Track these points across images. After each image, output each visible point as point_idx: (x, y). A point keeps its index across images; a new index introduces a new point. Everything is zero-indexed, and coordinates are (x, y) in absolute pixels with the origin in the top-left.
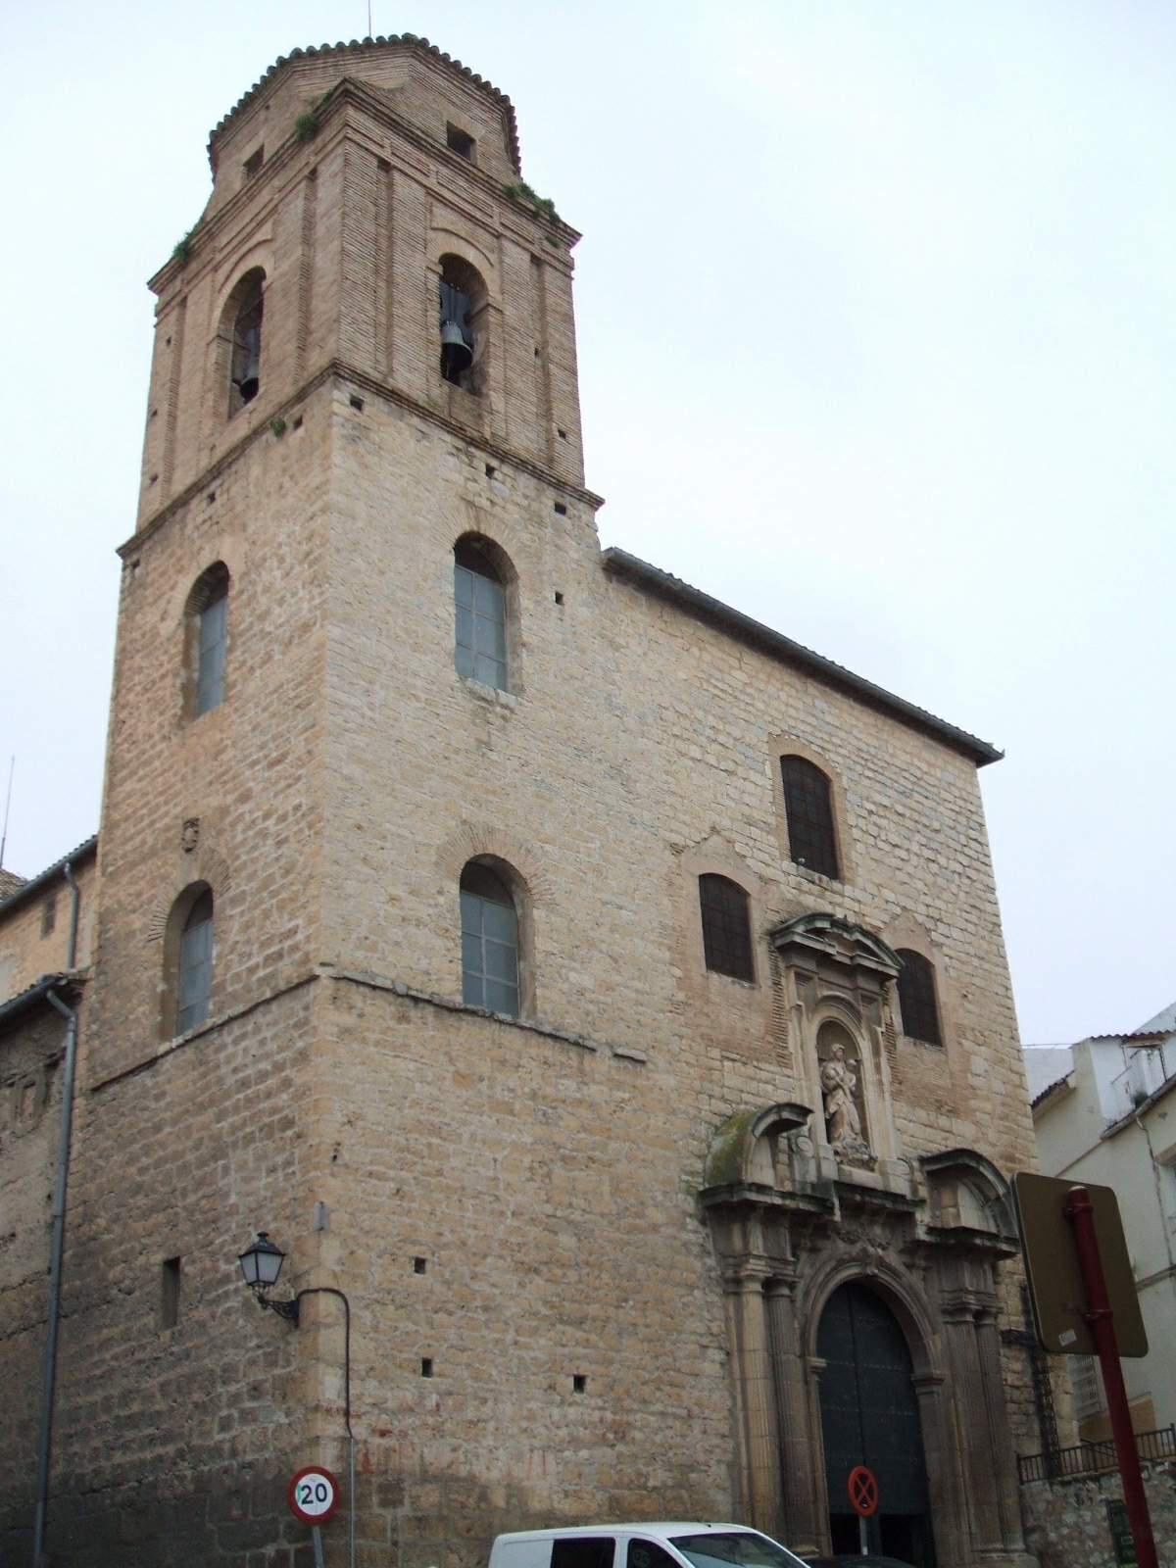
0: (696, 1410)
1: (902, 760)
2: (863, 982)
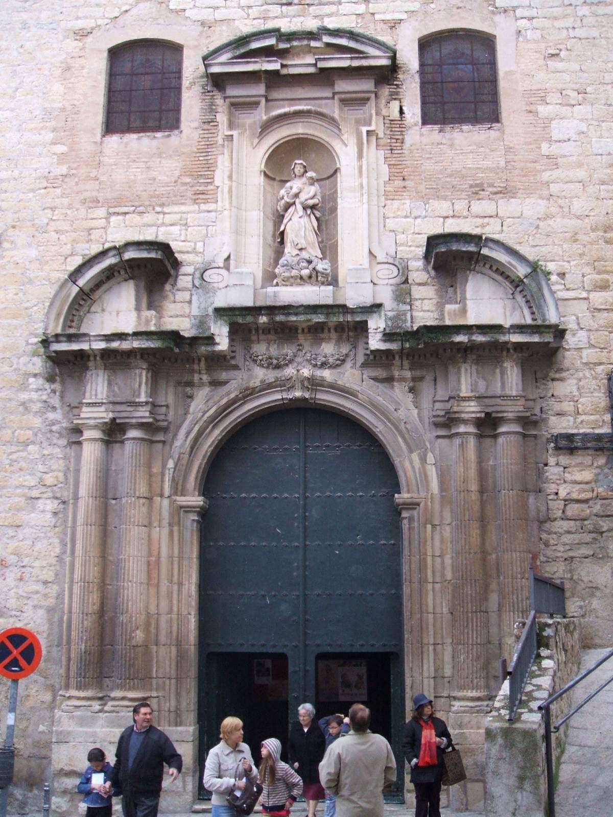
2: (343, 86)
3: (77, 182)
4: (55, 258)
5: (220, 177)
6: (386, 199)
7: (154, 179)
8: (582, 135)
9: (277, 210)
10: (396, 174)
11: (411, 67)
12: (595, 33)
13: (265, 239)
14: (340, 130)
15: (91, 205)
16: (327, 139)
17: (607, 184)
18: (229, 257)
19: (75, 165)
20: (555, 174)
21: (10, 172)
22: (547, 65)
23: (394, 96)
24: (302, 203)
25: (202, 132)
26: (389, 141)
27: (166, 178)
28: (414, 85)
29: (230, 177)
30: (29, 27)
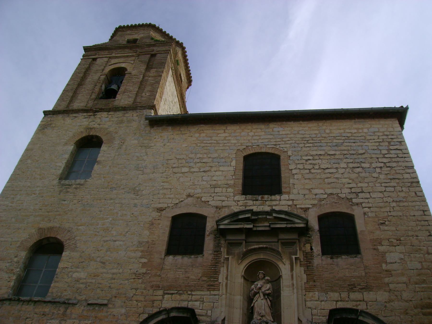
1: (336, 132)
2: (282, 236)
3: (150, 277)
4: (134, 314)
5: (221, 278)
6: (306, 291)
7: (188, 277)
8: (402, 260)
9: (250, 296)
10: (310, 279)
11: (315, 228)
12: (400, 214)
13: (243, 310)
14: (281, 257)
15: (155, 288)
16: (275, 261)
17: (418, 284)
18: (224, 319)
19: (150, 269)
20: (391, 279)
21: (118, 270)
22: (380, 228)
23: (309, 242)
24: (263, 293)
25: (213, 256)
26: (306, 263)
27: (194, 277)
28: (317, 237)
29: (227, 278)
30: (137, 206)
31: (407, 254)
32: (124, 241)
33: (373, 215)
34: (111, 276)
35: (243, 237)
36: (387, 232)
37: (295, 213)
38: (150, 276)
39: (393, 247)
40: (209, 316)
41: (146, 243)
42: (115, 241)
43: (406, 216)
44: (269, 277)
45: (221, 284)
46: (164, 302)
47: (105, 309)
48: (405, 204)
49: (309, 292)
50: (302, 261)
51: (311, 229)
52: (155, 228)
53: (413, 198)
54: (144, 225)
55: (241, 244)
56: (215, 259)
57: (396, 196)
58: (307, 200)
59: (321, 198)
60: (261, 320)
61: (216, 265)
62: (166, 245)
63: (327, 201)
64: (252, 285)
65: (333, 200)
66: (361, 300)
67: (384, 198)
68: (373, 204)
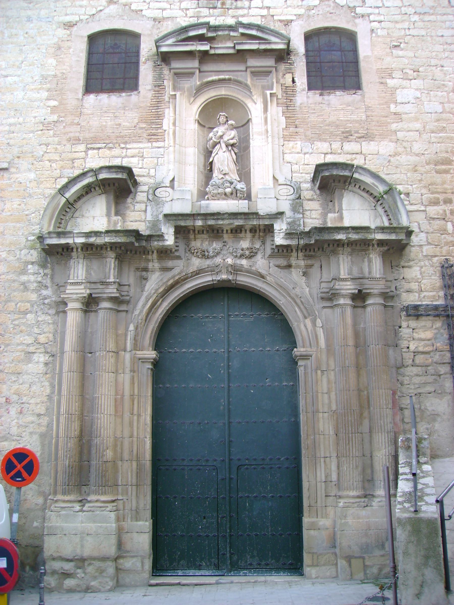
0: (15, 398)
2: (253, 62)
4: (48, 179)
5: (167, 124)
6: (284, 141)
7: (120, 125)
8: (418, 100)
9: (207, 148)
10: (291, 124)
11: (299, 51)
12: (423, 32)
13: (198, 168)
14: (251, 92)
15: (74, 142)
16: (242, 99)
17: (435, 133)
18: (174, 179)
20: (400, 125)
21: (16, 119)
22: (392, 52)
23: (290, 71)
24: (225, 142)
25: (154, 93)
26: (285, 101)
27: (128, 124)
28: (302, 63)
29: (174, 124)
31: (426, 92)
32: (19, 76)
33: (384, 32)
34: (7, 128)
35: (196, 64)
36: (402, 58)
37: (272, 28)
38: (64, 125)
39: (407, 81)
40: (152, 176)
41: (53, 77)
42: (7, 76)
43: (431, 36)
44: (234, 121)
45: (166, 132)
46: (87, 160)
47: (6, 175)
48: (432, 18)
49: (289, 141)
50: (279, 99)
51: (293, 52)
52: (65, 54)
53: (444, 9)
54: (46, 50)
55: (193, 74)
56: (156, 98)
57: (421, 5)
58: (290, 9)
59: (310, 5)
60: (224, 180)
61: (159, 105)
62: (83, 79)
63: (319, 11)
64: (211, 132)
65: (328, 9)
66: (358, 152)
67: (402, 8)
68: (386, 17)
